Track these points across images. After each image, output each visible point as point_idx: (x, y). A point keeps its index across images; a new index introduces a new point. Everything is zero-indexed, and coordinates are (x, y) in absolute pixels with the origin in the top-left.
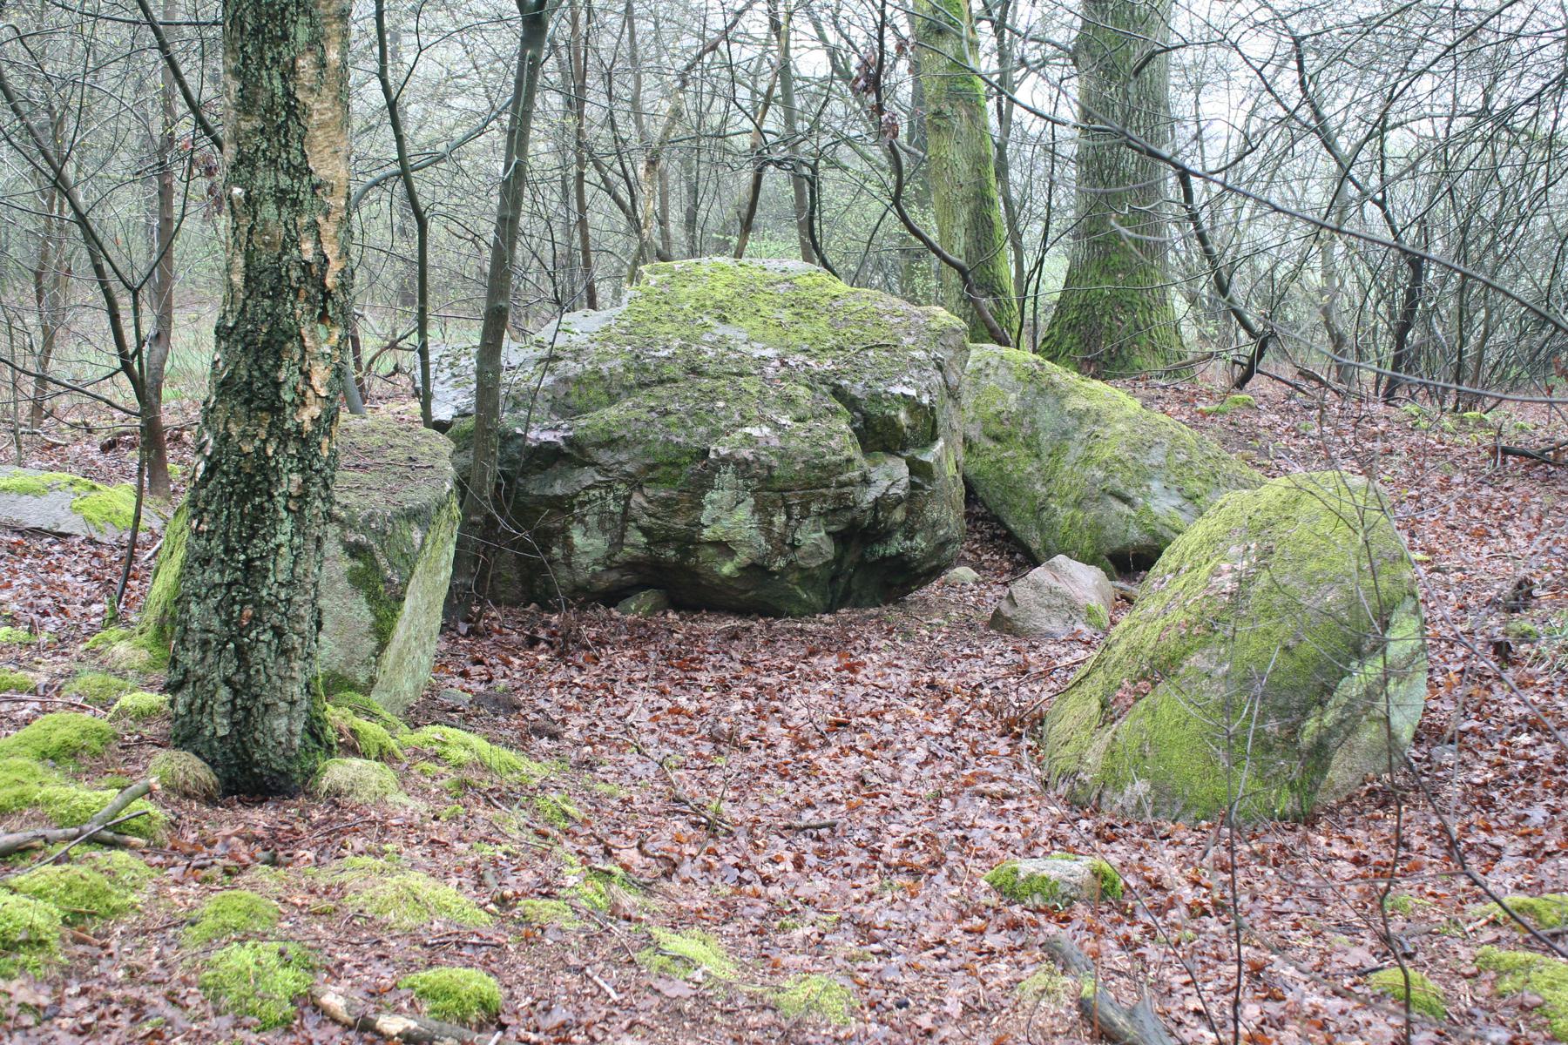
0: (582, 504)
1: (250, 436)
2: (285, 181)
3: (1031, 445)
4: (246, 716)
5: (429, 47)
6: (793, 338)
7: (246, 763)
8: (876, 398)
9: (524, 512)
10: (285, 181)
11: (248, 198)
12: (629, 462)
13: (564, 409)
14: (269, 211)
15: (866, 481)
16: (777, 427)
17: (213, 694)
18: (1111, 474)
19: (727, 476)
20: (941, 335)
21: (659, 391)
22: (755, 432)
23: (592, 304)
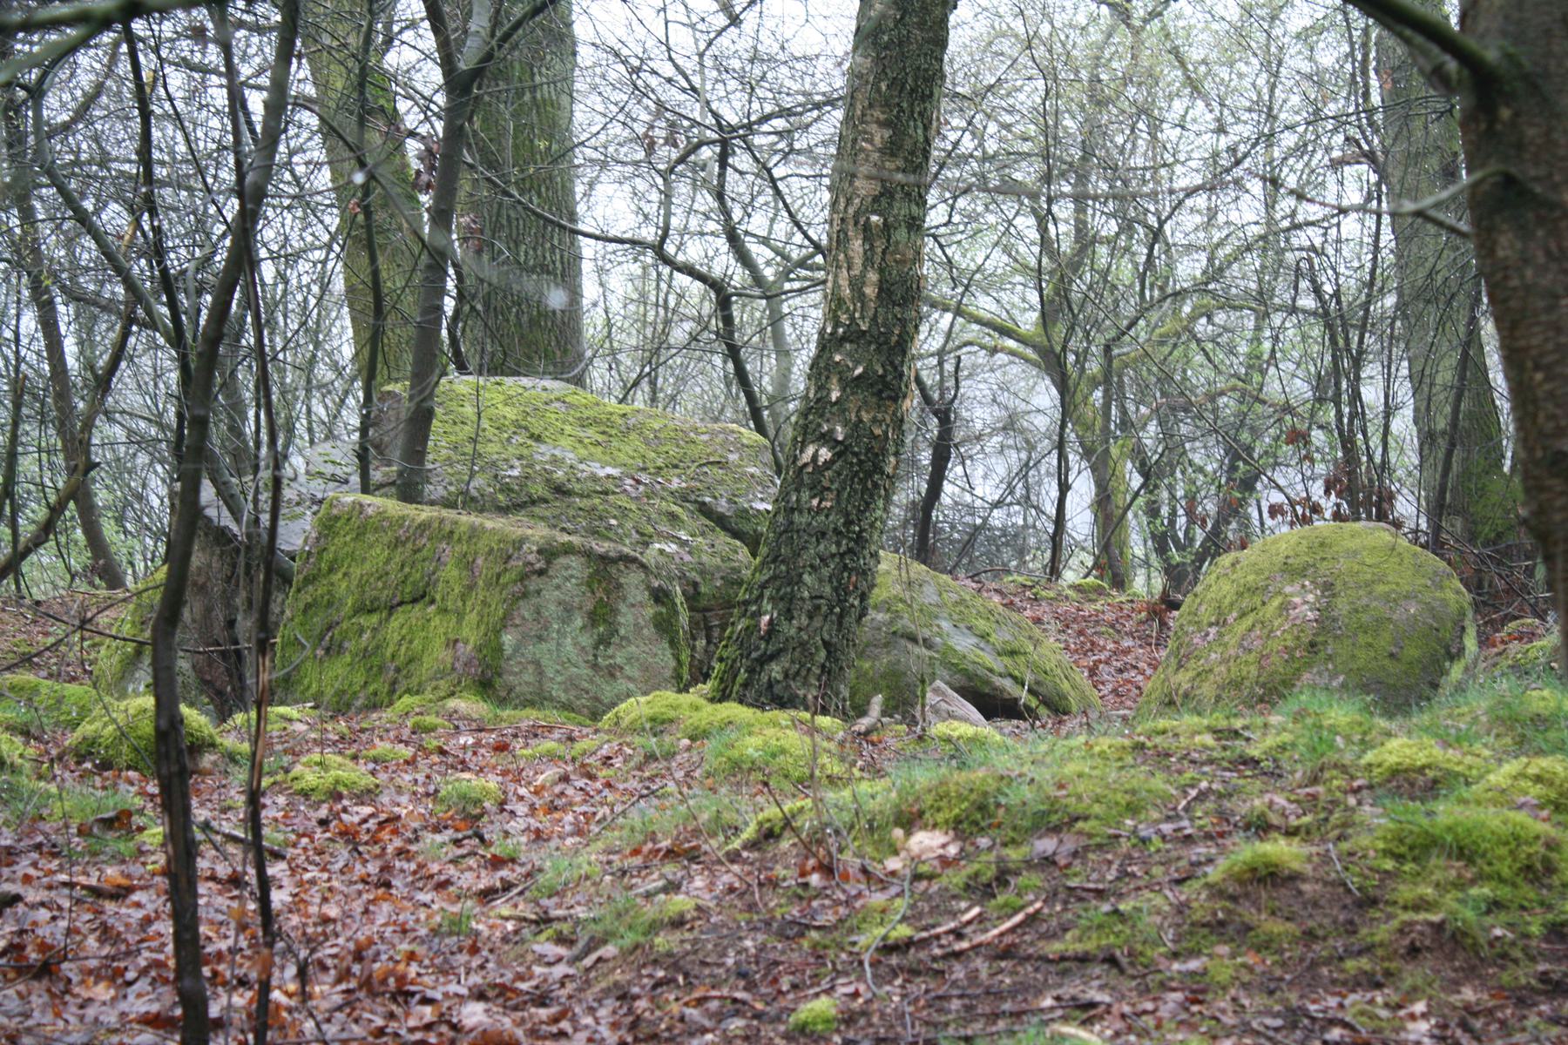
11: (885, 223)
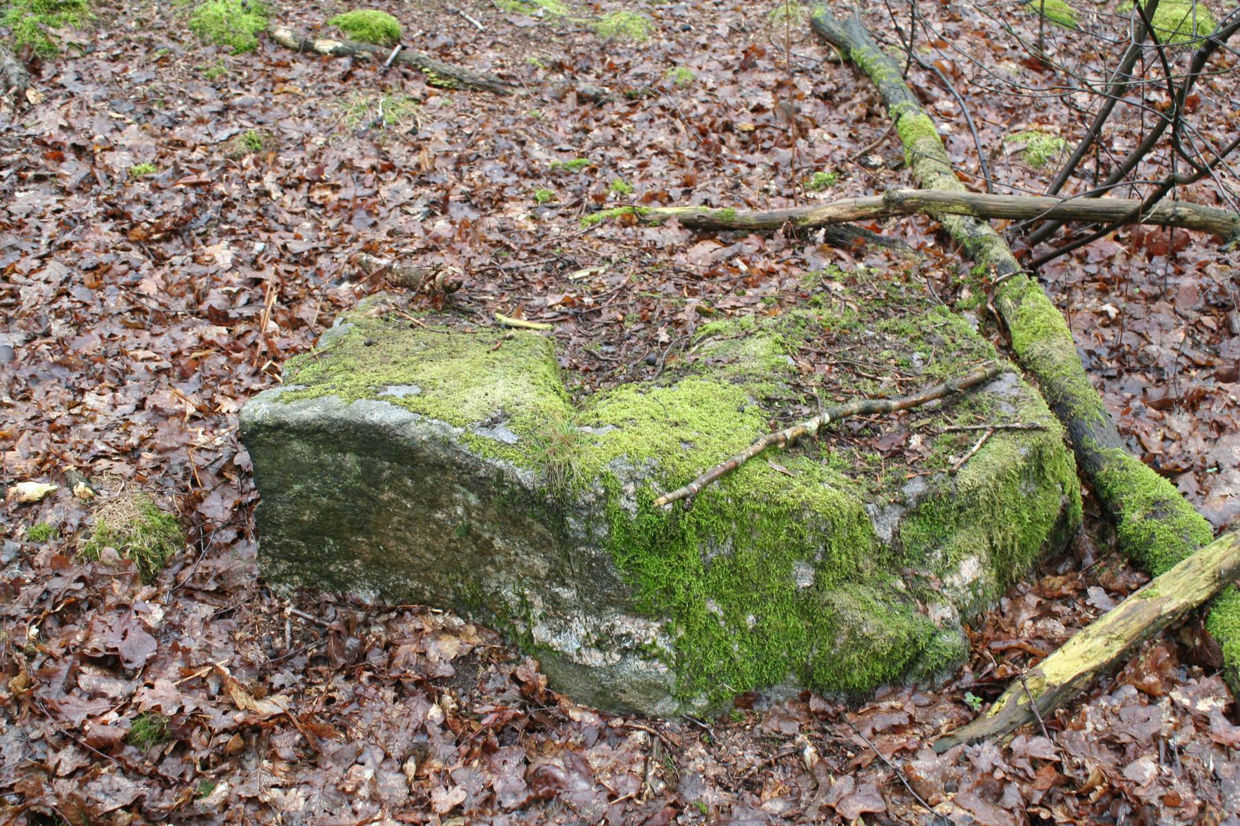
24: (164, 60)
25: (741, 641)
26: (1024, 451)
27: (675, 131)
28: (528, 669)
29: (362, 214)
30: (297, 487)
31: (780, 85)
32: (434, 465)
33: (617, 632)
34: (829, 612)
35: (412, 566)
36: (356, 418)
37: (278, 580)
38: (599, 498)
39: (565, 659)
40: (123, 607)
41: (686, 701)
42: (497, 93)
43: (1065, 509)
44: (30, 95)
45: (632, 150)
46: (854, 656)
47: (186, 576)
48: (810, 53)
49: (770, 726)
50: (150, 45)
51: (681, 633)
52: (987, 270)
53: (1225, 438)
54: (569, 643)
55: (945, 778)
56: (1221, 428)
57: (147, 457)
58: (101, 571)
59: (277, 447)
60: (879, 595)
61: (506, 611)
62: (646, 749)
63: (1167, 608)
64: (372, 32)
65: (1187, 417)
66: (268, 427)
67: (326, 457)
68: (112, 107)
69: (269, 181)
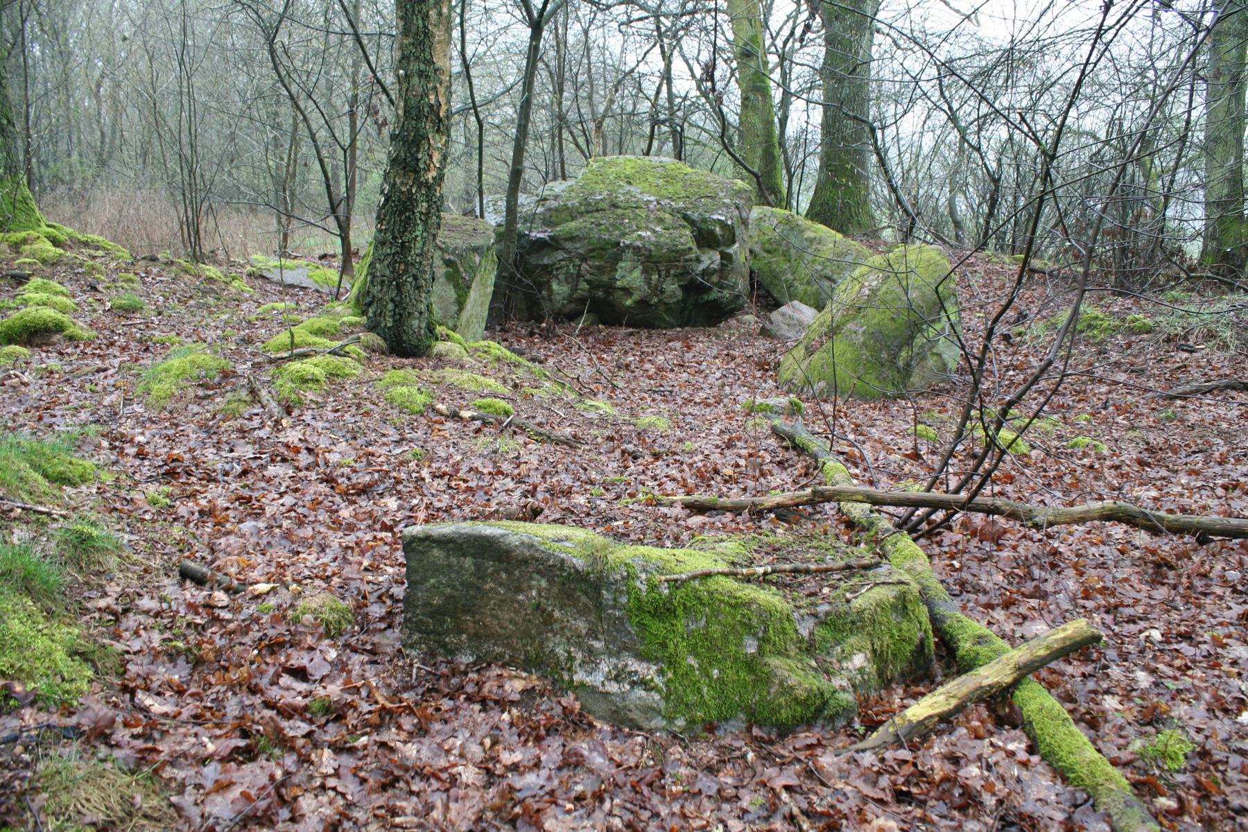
0: (557, 269)
1: (404, 184)
2: (423, 67)
3: (786, 254)
4: (401, 317)
5: (489, 31)
6: (663, 192)
7: (399, 341)
8: (704, 220)
9: (528, 272)
10: (423, 67)
12: (581, 248)
13: (548, 222)
14: (415, 80)
15: (698, 260)
16: (654, 232)
17: (385, 306)
18: (825, 268)
19: (629, 254)
20: (739, 192)
21: (596, 214)
22: (644, 234)
23: (564, 178)
24: (367, 414)
25: (709, 686)
26: (894, 593)
27: (682, 471)
28: (569, 700)
29: (482, 493)
30: (432, 581)
31: (751, 455)
32: (521, 561)
33: (629, 669)
34: (766, 669)
35: (499, 635)
36: (476, 533)
37: (412, 647)
38: (623, 578)
39: (594, 690)
40: (311, 649)
41: (671, 720)
42: (571, 447)
43: (922, 641)
44: (284, 422)
45: (654, 478)
46: (782, 700)
47: (353, 641)
48: (772, 442)
49: (727, 741)
50: (359, 406)
51: (670, 675)
52: (876, 533)
53: (1027, 623)
54: (596, 679)
55: (840, 770)
56: (1025, 618)
57: (336, 580)
58: (301, 629)
59: (423, 553)
60: (799, 665)
61: (558, 663)
62: (642, 745)
63: (986, 682)
64: (496, 410)
65: (1002, 612)
66: (420, 539)
67: (453, 560)
68: (332, 432)
69: (425, 473)
